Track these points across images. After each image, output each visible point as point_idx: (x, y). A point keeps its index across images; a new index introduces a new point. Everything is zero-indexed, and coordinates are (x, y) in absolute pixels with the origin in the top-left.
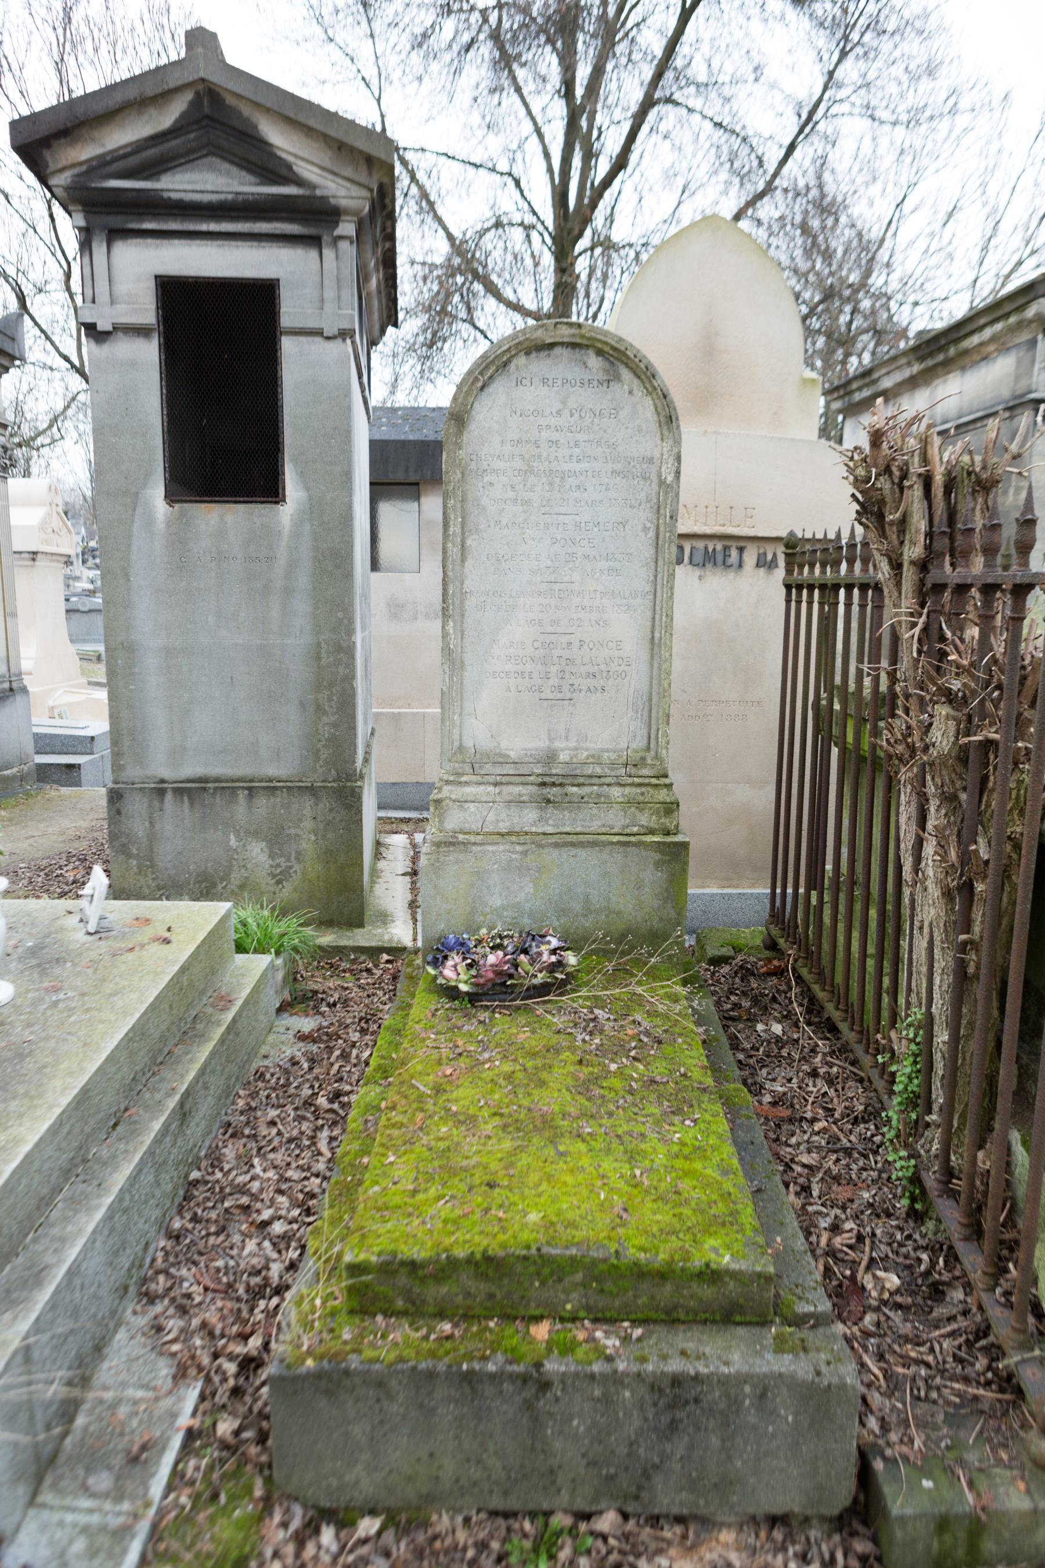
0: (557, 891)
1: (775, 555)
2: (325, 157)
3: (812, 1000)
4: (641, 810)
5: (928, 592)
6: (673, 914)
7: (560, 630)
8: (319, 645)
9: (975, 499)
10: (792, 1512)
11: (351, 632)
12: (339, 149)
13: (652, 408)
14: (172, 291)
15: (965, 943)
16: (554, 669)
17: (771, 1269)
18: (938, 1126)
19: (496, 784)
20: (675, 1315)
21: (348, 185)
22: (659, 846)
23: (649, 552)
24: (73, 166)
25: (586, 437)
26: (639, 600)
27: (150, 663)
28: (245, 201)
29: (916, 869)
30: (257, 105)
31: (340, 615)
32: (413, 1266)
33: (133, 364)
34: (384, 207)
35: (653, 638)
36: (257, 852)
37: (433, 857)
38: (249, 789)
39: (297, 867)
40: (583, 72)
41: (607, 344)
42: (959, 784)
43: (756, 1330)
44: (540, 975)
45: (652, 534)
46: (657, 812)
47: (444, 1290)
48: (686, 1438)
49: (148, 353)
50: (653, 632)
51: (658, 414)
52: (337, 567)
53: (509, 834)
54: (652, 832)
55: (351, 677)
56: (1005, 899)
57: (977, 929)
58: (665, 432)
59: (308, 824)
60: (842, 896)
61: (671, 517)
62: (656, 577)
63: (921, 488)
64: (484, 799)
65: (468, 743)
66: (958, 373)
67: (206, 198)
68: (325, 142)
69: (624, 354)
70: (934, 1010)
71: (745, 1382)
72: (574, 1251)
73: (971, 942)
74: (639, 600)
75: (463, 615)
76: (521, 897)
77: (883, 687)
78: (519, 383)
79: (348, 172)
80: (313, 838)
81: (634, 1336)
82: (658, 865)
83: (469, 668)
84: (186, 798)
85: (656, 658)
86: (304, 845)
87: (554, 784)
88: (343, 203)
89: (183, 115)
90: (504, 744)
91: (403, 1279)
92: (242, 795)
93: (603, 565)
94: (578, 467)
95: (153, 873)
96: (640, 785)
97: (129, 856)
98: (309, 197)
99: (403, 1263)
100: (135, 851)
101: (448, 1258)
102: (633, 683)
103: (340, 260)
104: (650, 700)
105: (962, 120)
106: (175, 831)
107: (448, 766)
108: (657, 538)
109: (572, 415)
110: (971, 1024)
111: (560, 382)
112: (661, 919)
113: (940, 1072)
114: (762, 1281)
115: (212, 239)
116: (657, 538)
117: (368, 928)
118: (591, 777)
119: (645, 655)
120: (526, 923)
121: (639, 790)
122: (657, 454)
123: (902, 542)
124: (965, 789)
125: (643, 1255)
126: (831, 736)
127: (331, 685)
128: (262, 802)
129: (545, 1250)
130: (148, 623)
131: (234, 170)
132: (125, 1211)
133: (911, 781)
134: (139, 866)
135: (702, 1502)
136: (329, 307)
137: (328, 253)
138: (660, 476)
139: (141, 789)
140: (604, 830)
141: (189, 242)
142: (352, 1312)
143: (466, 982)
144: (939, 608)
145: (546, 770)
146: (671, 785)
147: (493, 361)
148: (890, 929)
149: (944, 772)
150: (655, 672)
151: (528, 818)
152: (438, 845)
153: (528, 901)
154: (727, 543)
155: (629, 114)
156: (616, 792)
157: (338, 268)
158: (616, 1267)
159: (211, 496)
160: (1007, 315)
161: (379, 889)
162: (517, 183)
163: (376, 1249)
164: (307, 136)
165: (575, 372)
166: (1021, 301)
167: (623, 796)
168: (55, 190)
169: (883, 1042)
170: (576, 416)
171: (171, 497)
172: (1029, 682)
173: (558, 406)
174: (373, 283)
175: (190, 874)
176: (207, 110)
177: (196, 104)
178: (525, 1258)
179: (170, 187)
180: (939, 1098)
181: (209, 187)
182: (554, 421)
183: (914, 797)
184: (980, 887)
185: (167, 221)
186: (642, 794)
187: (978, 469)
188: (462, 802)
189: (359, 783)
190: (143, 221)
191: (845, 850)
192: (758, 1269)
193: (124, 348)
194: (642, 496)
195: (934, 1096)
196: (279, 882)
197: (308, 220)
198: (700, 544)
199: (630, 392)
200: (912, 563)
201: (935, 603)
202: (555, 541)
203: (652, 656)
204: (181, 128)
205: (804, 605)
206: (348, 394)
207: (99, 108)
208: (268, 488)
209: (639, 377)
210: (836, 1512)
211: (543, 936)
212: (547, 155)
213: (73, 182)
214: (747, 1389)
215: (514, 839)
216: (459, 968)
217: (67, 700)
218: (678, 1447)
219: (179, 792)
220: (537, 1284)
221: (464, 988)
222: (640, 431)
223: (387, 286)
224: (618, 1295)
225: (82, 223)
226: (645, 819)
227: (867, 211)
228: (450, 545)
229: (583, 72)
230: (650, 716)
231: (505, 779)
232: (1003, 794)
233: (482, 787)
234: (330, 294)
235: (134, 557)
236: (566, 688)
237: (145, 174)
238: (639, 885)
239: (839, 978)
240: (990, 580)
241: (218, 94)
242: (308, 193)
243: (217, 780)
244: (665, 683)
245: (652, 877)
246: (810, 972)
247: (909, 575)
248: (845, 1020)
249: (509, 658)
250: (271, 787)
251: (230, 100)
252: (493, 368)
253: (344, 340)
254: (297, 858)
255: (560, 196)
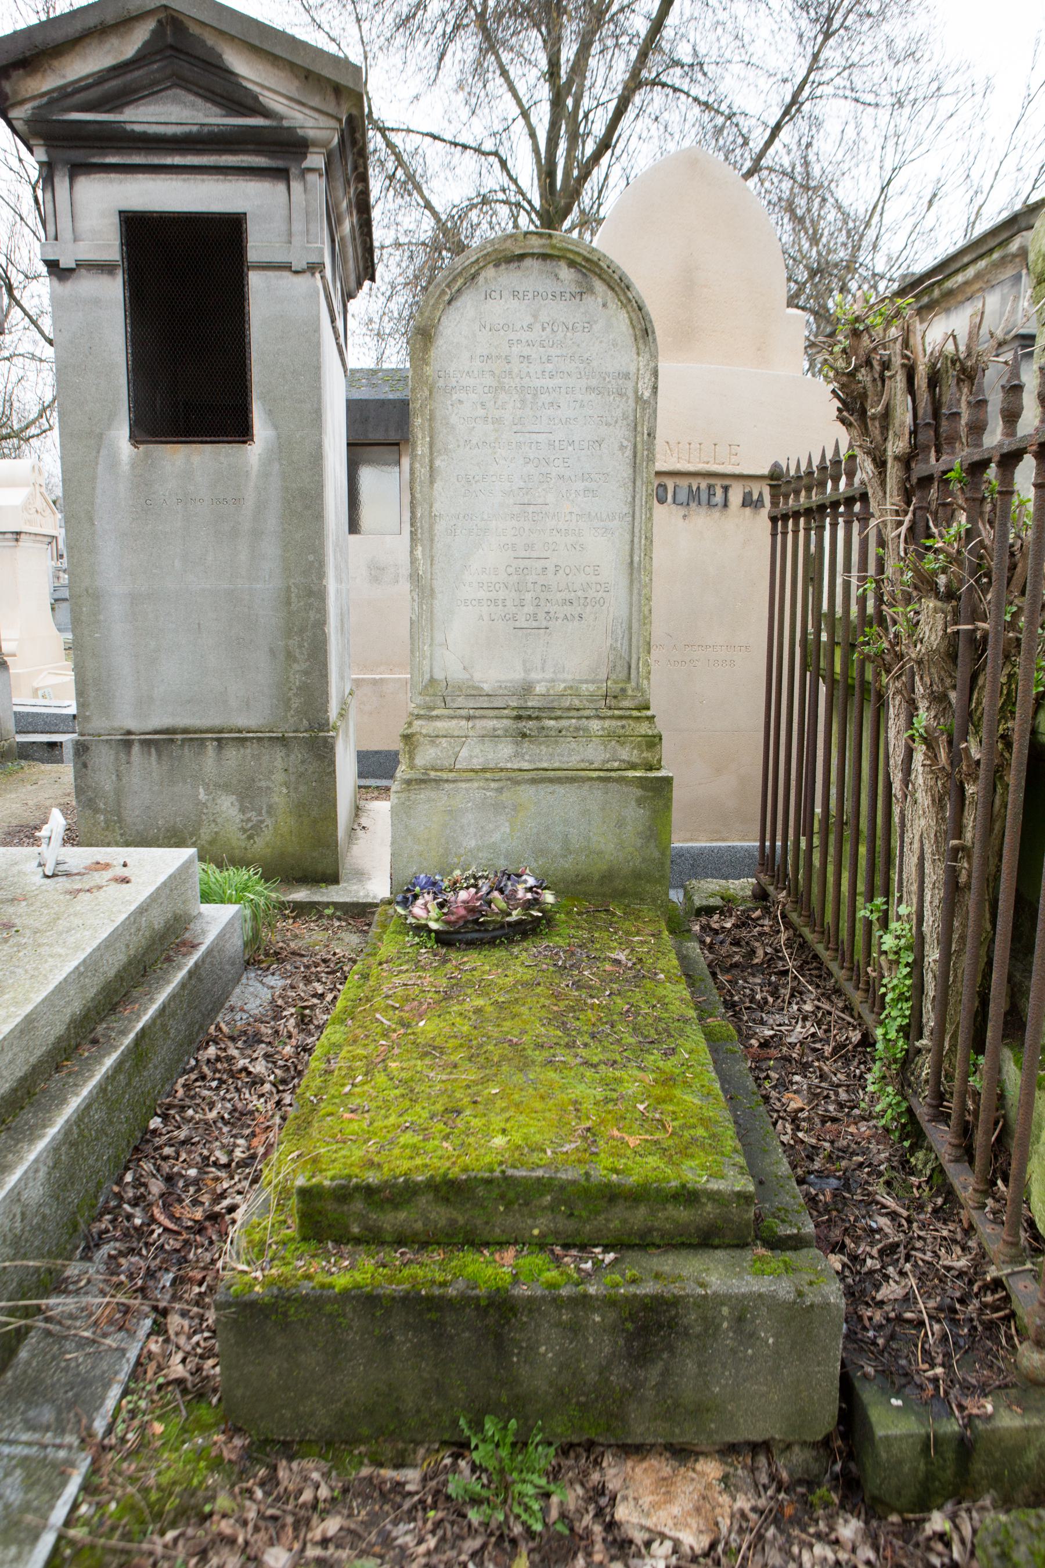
0: (535, 830)
1: (761, 494)
2: (290, 86)
3: (804, 946)
4: (622, 744)
5: (912, 489)
6: (656, 854)
7: (534, 555)
8: (288, 588)
9: (960, 390)
10: (773, 1439)
11: (321, 575)
12: (306, 78)
13: (627, 321)
14: (139, 229)
15: (956, 850)
16: (528, 596)
17: (751, 1188)
18: (929, 1051)
19: (469, 718)
20: (649, 1240)
21: (316, 115)
22: (641, 782)
23: (626, 472)
24: (33, 98)
25: (559, 352)
26: (616, 522)
27: (116, 609)
28: (211, 134)
29: (906, 781)
30: (221, 33)
31: (311, 558)
32: (369, 1191)
33: (96, 302)
34: (354, 142)
35: (632, 562)
36: (227, 806)
37: (403, 795)
38: (219, 740)
39: (269, 822)
40: (568, 53)
41: (578, 254)
42: (948, 682)
43: (737, 1253)
44: (514, 913)
45: (629, 453)
46: (639, 746)
47: (402, 1215)
48: (661, 1363)
49: (112, 290)
50: (632, 557)
51: (634, 327)
52: (307, 507)
53: (484, 770)
54: (633, 767)
55: (321, 623)
56: (997, 802)
57: (969, 835)
58: (641, 346)
59: (279, 777)
60: (832, 838)
61: (649, 435)
62: (634, 498)
63: (904, 380)
64: (456, 734)
65: (439, 675)
66: (943, 315)
67: (170, 130)
68: (292, 71)
69: (597, 265)
70: (925, 928)
71: (723, 1304)
72: (540, 1173)
73: (963, 848)
74: (616, 522)
75: (432, 540)
76: (496, 837)
77: (870, 610)
78: (488, 296)
79: (316, 102)
80: (285, 791)
81: (607, 1260)
82: (639, 802)
83: (439, 596)
84: (153, 750)
85: (636, 585)
86: (276, 799)
87: (530, 718)
88: (311, 134)
89: (146, 44)
90: (478, 676)
91: (358, 1205)
92: (211, 748)
93: (580, 485)
94: (551, 383)
95: (121, 828)
96: (621, 718)
97: (96, 811)
98: (276, 128)
99: (357, 1188)
100: (102, 806)
101: (406, 1181)
102: (611, 609)
103: (310, 192)
104: (630, 628)
105: (946, 105)
106: (142, 782)
107: (419, 700)
108: (635, 457)
109: (544, 329)
110: (962, 938)
111: (530, 296)
112: (644, 860)
113: (931, 994)
114: (742, 1201)
115: (176, 173)
116: (635, 457)
117: (342, 885)
118: (569, 709)
119: (624, 582)
120: (502, 864)
121: (619, 723)
122: (633, 369)
123: (886, 439)
124: (954, 687)
125: (615, 1176)
126: (818, 668)
127: (302, 630)
128: (232, 754)
129: (510, 1172)
130: (113, 570)
131: (199, 101)
132: (72, 1144)
133: (898, 692)
134: (106, 821)
135: (677, 1431)
136: (297, 240)
137: (296, 186)
138: (636, 392)
139: (107, 741)
140: (583, 765)
141: (153, 176)
142: (305, 1239)
143: (437, 920)
144: (925, 505)
145: (522, 703)
146: (653, 717)
147: (460, 274)
148: (880, 862)
149: (933, 670)
150: (635, 598)
151: (503, 753)
152: (408, 782)
153: (504, 841)
154: (712, 481)
155: (615, 95)
156: (595, 725)
157: (306, 201)
158: (586, 1190)
159: (177, 436)
160: (991, 251)
161: (356, 850)
162: (503, 164)
163: (330, 1174)
164: (273, 65)
165: (548, 285)
166: (1005, 235)
167: (603, 729)
168: (14, 122)
169: (874, 974)
170: (549, 330)
171: (135, 439)
172: (1019, 570)
173: (529, 319)
174: (347, 226)
175: (159, 829)
176: (170, 40)
177: (158, 34)
178: (488, 1182)
179: (133, 119)
180: (930, 1020)
181: (173, 120)
182: (525, 336)
183: (904, 705)
184: (970, 789)
185: (130, 155)
186: (623, 727)
187: (962, 356)
188: (434, 738)
189: (331, 734)
190: (106, 155)
191: (833, 791)
192: (737, 1188)
193: (88, 285)
194: (619, 413)
195: (924, 1020)
196: (250, 837)
197: (277, 152)
198: (684, 483)
199: (604, 305)
200: (897, 458)
201: (920, 500)
202: (527, 461)
203: (631, 582)
204: (144, 57)
205: (790, 536)
206: (317, 330)
207: (59, 35)
208: (236, 427)
209: (613, 289)
210: (819, 1438)
211: (519, 876)
212: (533, 135)
213: (33, 114)
214: (725, 1311)
215: (488, 775)
216: (429, 906)
217: (46, 684)
218: (653, 1374)
219: (146, 744)
220: (502, 1208)
221: (434, 926)
222: (615, 345)
223: (362, 234)
224: (589, 1219)
225: (44, 158)
226: (625, 753)
227: (855, 193)
228: (417, 465)
229: (568, 53)
230: (630, 645)
231: (478, 713)
232: (993, 691)
233: (454, 722)
234: (298, 226)
235: (98, 501)
236: (541, 616)
237: (108, 107)
238: (621, 824)
239: (829, 918)
240: (976, 458)
241: (181, 22)
242: (274, 123)
243: (185, 731)
244: (646, 610)
245: (635, 815)
246: (800, 915)
247: (893, 471)
248: (834, 959)
249: (481, 584)
250: (241, 739)
251: (194, 29)
252: (460, 281)
253: (313, 274)
254: (268, 812)
255: (547, 172)
